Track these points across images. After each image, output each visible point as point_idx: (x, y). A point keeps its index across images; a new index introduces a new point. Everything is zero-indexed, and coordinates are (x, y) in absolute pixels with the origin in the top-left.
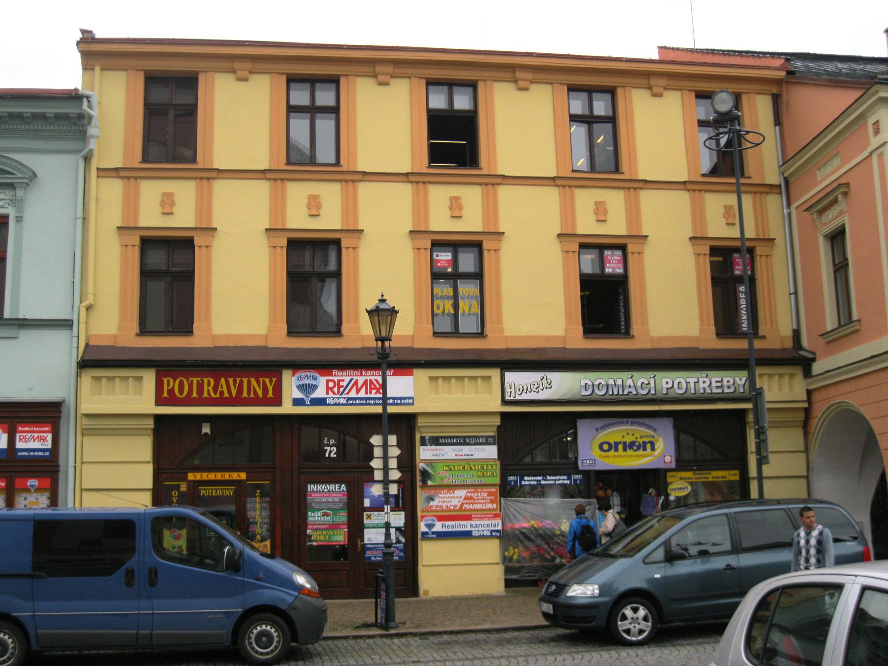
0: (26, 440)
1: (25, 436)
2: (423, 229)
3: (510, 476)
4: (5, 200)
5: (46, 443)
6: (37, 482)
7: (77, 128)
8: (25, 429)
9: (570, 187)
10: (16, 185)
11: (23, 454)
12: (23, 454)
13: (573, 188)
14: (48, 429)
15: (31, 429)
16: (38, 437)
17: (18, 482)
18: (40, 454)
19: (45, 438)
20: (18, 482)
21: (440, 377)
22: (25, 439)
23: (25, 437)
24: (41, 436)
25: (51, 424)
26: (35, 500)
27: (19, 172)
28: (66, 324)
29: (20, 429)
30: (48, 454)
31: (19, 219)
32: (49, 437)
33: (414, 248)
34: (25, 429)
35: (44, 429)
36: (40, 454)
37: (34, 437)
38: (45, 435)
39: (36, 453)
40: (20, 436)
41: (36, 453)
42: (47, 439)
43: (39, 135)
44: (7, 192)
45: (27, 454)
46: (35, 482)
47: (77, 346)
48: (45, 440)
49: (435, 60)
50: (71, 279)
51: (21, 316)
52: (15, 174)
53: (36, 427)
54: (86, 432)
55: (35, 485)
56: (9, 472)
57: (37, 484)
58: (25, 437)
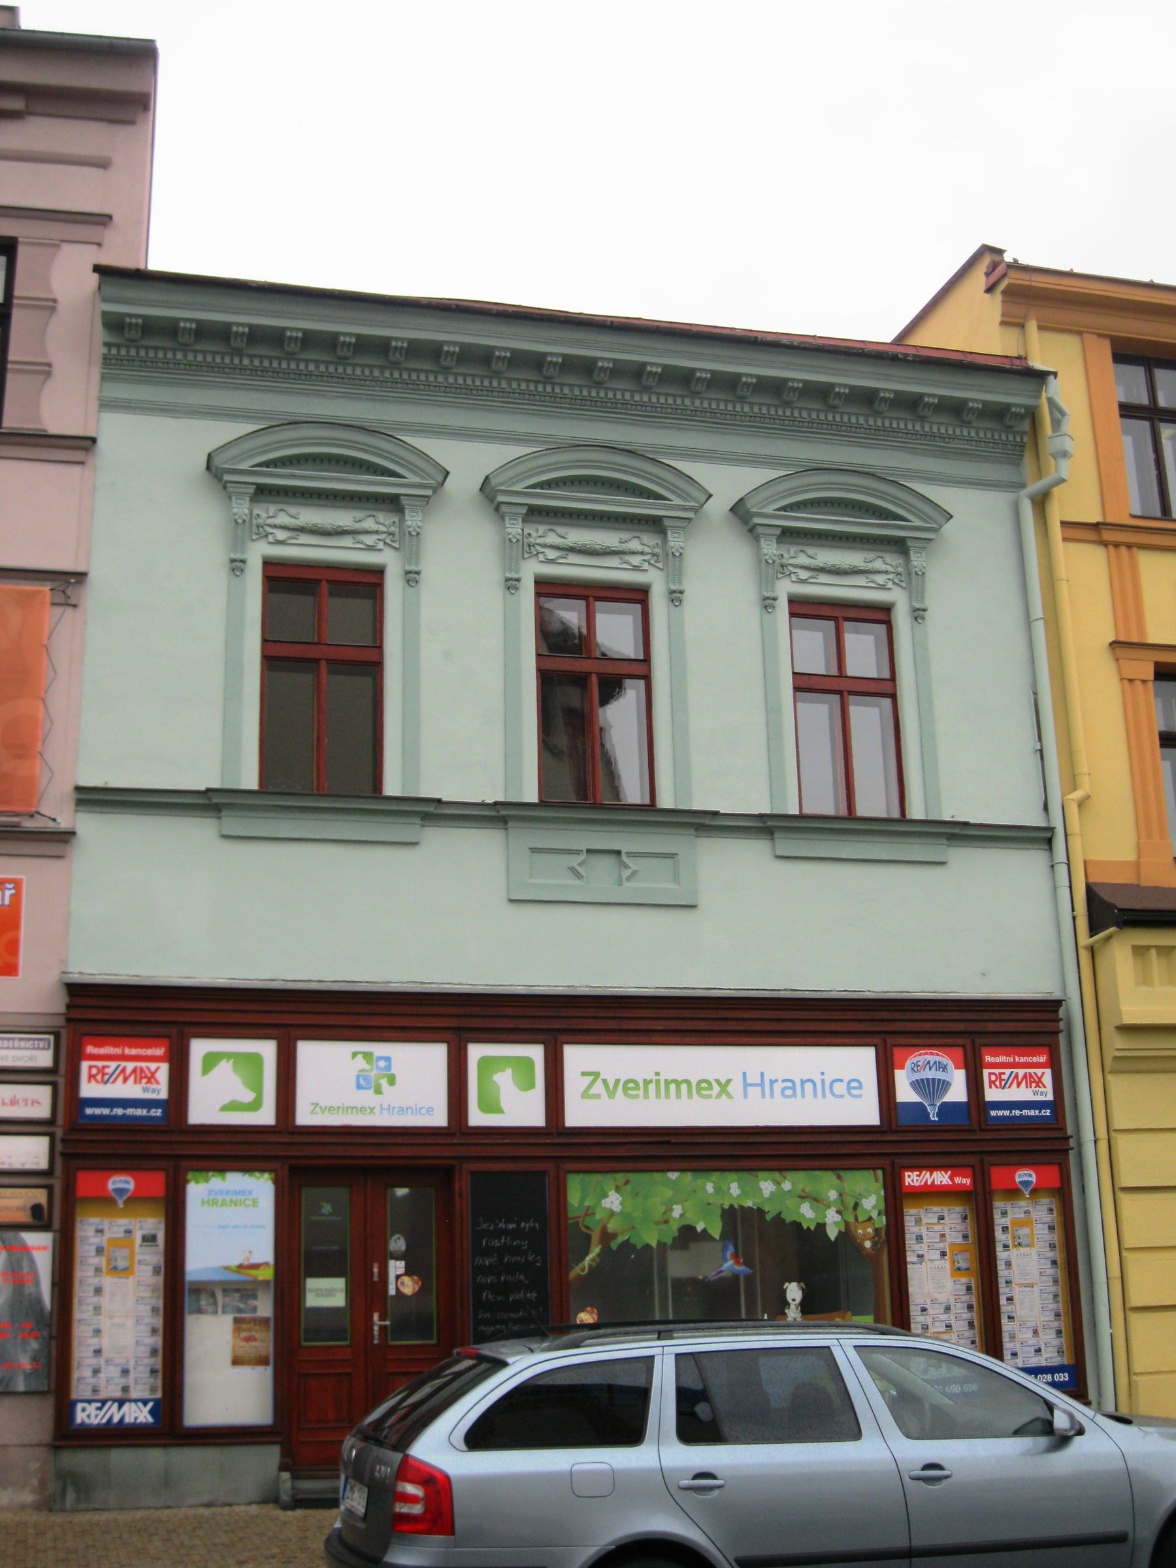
0: (102, 1077)
1: (104, 1067)
2: (1135, 640)
3: (912, 1168)
4: (377, 532)
5: (155, 1086)
6: (1034, 1175)
7: (1011, 438)
8: (998, 1060)
9: (1129, 546)
10: (667, 522)
11: (1000, 1113)
12: (1000, 1113)
13: (1135, 550)
14: (159, 1052)
15: (1010, 1059)
16: (134, 1071)
17: (997, 1175)
18: (1033, 1113)
19: (153, 1074)
20: (85, 1182)
21: (1152, 946)
22: (104, 1074)
23: (102, 1071)
24: (142, 1070)
25: (166, 1041)
26: (1022, 1216)
27: (411, 470)
28: (1042, 838)
29: (90, 1049)
30: (158, 1112)
31: (412, 578)
32: (163, 1072)
33: (1122, 679)
34: (998, 1060)
35: (1035, 1059)
36: (1033, 1113)
37: (1016, 1076)
38: (153, 1066)
39: (130, 1111)
40: (91, 1067)
41: (130, 1111)
42: (1043, 1080)
43: (466, 395)
44: (381, 517)
45: (106, 1111)
46: (127, 1182)
47: (1068, 884)
48: (151, 1078)
49: (1132, 301)
50: (1031, 743)
51: (424, 793)
52: (908, 521)
53: (131, 1047)
54: (1128, 1065)
55: (1031, 1182)
56: (170, 1157)
57: (1034, 1179)
58: (102, 1071)
